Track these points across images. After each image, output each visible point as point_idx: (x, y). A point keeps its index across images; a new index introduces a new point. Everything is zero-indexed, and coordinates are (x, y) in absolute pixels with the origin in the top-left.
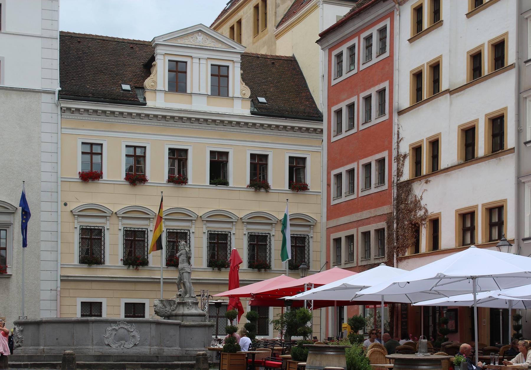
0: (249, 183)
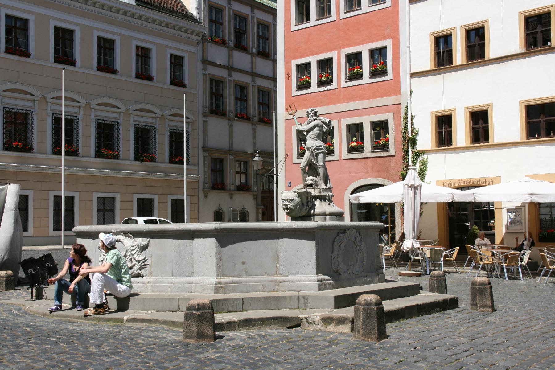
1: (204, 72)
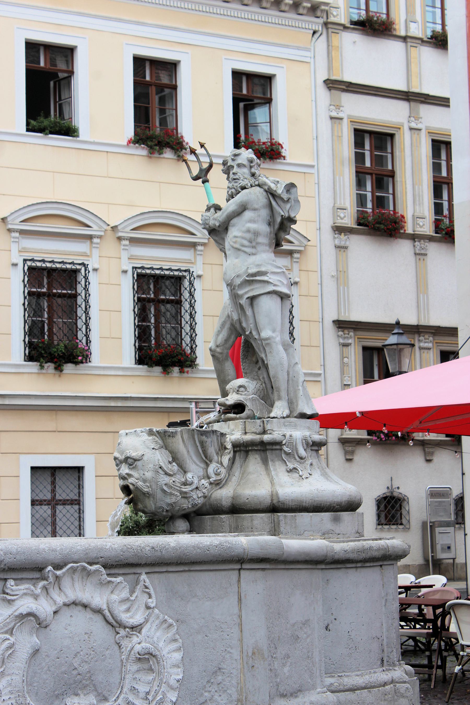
0: (133, 134)
1: (334, 114)
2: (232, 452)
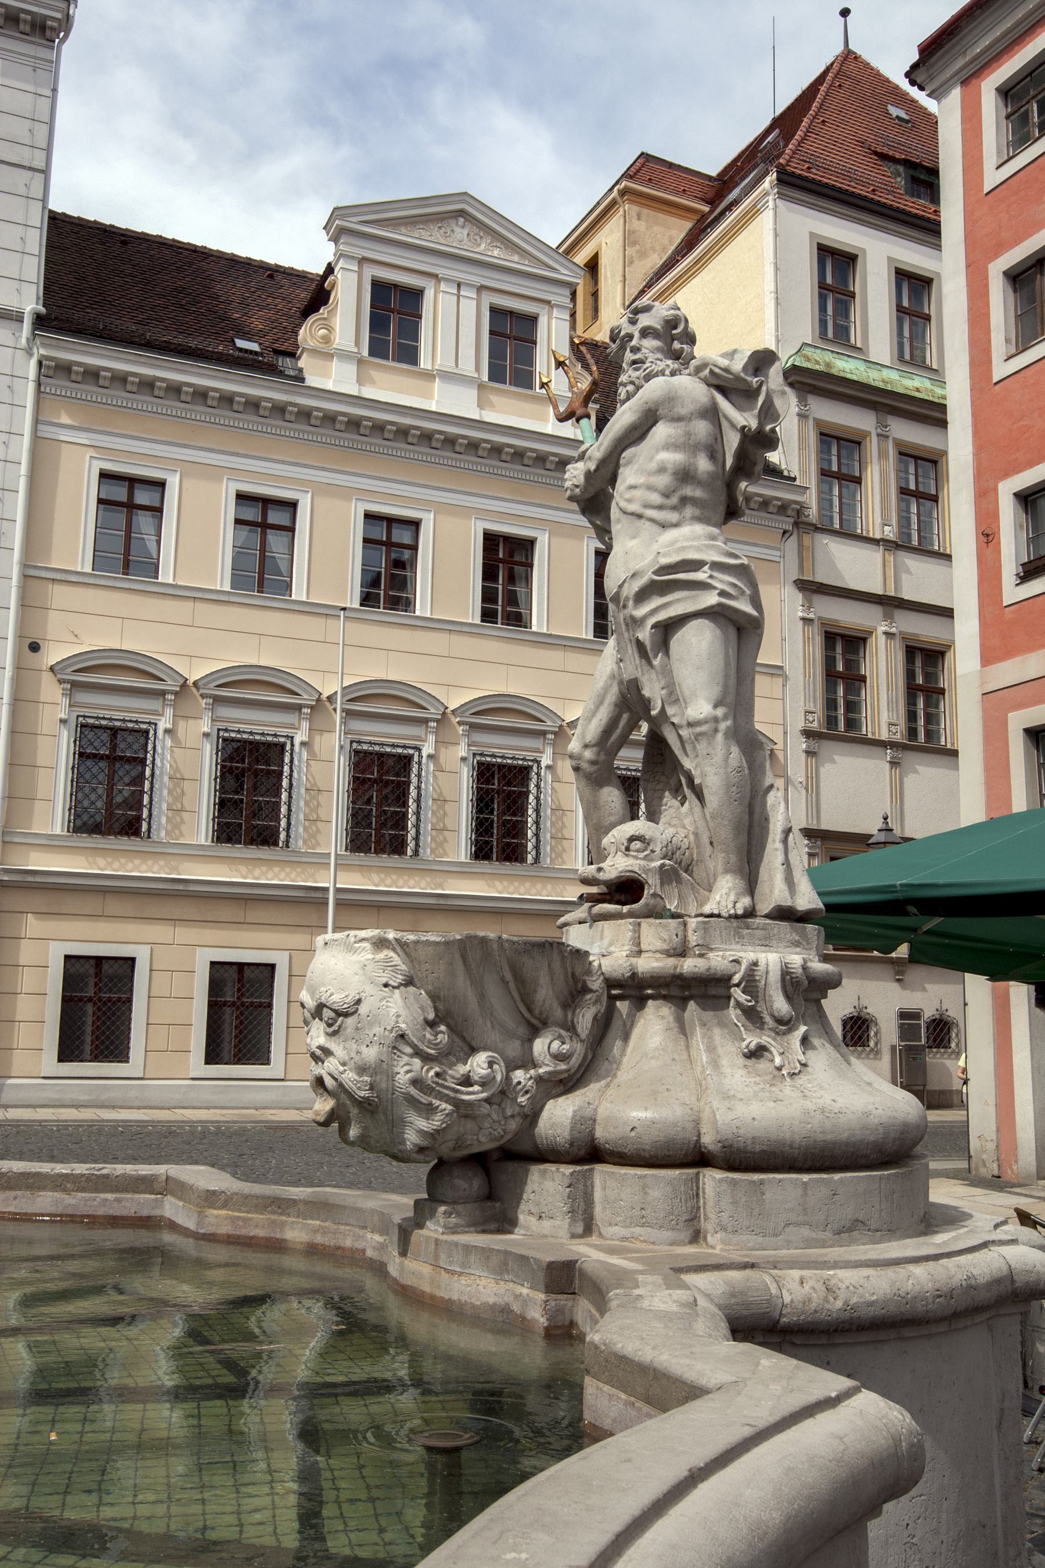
2: (605, 998)
